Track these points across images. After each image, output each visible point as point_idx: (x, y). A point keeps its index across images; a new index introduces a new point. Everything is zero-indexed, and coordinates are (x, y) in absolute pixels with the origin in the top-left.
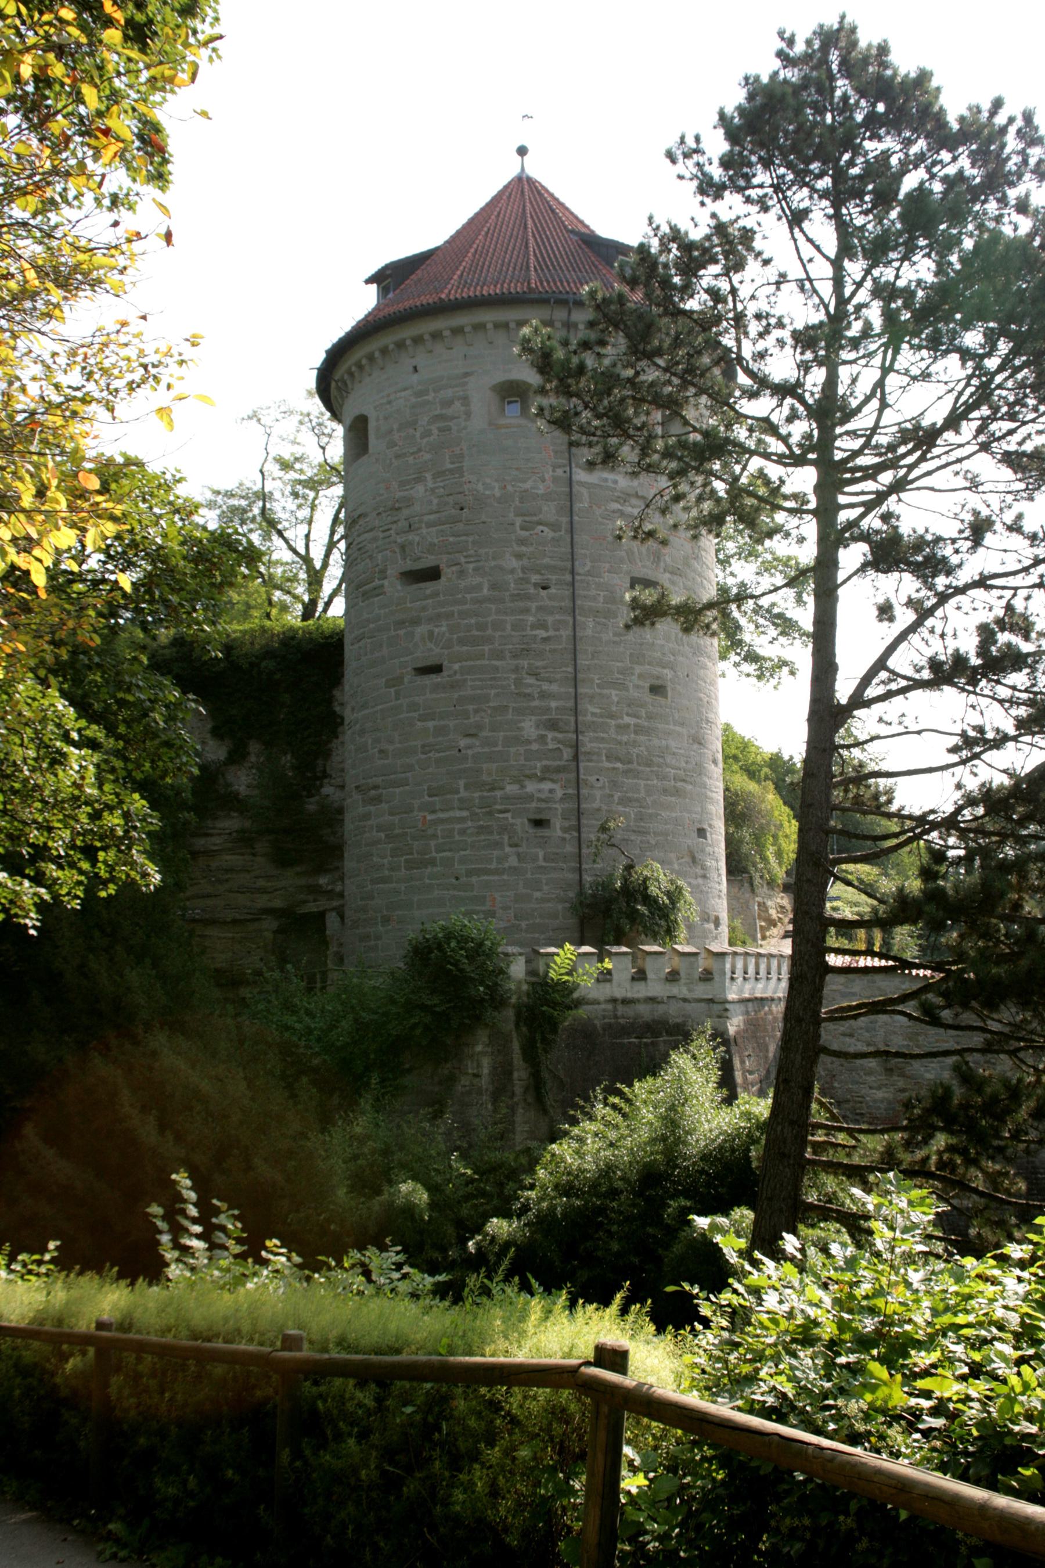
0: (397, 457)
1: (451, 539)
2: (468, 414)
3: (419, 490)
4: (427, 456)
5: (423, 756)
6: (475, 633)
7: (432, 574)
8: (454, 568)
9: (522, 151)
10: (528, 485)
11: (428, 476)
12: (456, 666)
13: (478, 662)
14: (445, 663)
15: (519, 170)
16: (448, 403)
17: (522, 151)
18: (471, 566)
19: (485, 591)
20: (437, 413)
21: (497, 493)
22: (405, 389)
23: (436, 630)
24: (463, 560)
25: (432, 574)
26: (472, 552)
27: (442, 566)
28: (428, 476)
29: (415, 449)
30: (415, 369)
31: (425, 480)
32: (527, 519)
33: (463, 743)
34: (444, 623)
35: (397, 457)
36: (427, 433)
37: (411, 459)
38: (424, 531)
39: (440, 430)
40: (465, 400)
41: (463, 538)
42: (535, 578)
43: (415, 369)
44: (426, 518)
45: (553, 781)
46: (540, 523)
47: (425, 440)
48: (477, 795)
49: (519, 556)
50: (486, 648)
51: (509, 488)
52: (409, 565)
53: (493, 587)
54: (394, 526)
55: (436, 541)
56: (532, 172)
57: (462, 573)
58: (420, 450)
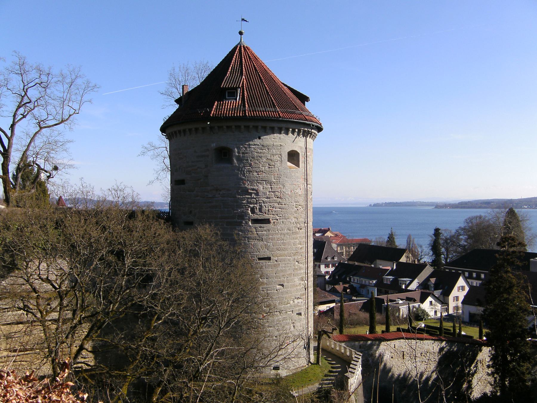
17: (241, 33)
27: (271, 219)
56: (246, 43)
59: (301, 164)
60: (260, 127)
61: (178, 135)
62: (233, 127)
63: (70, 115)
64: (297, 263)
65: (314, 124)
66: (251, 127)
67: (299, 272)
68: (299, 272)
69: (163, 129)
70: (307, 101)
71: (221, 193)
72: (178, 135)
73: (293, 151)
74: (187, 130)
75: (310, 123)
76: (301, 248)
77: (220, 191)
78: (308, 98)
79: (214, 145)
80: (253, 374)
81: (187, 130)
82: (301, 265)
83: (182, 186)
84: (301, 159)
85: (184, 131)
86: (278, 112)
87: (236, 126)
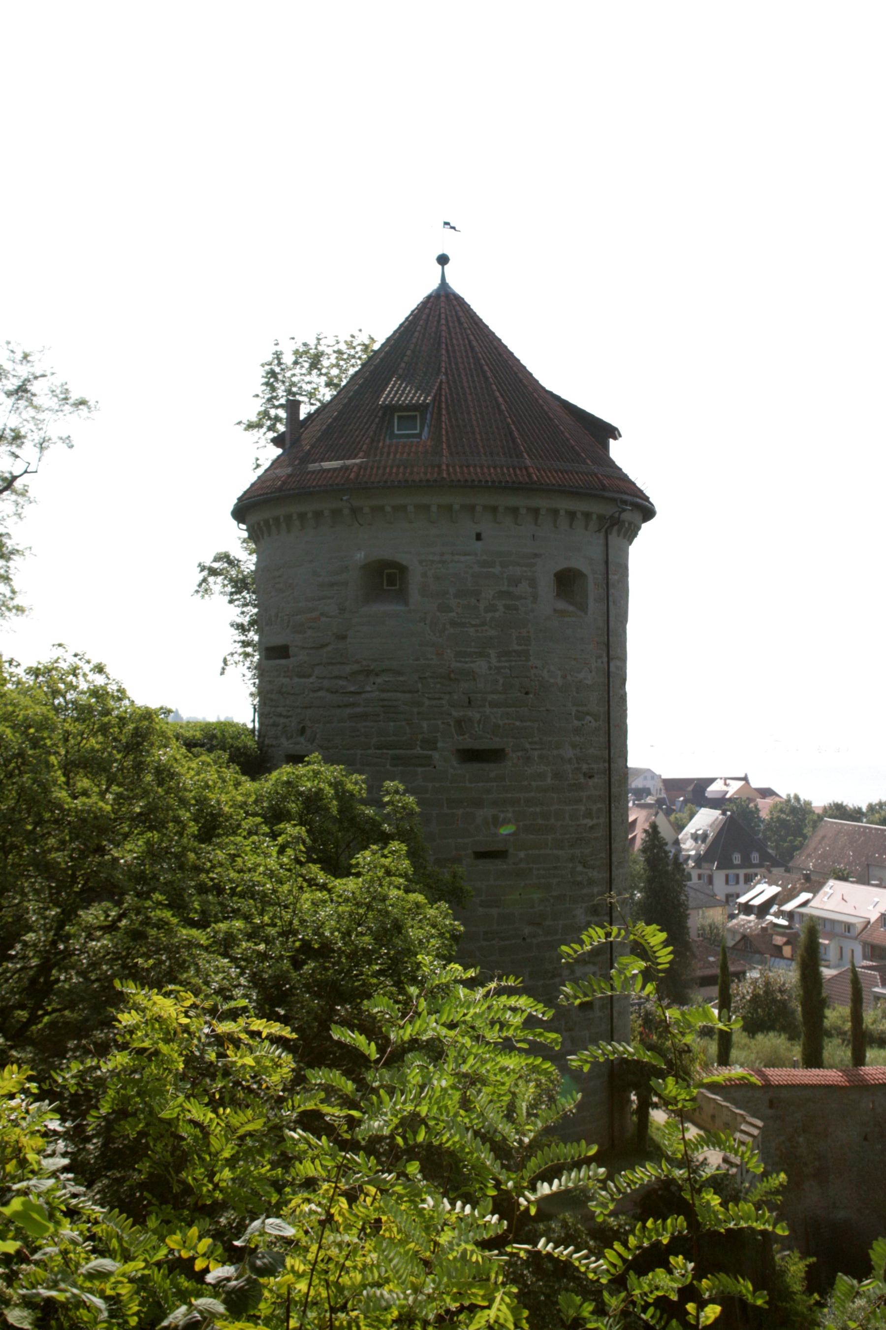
0: (453, 623)
1: (518, 723)
2: (535, 598)
3: (480, 666)
4: (492, 633)
5: (485, 943)
6: (540, 821)
7: (494, 756)
8: (519, 754)
9: (443, 260)
10: (581, 676)
11: (492, 653)
12: (522, 854)
13: (542, 852)
14: (511, 850)
15: (439, 281)
16: (515, 581)
17: (443, 260)
18: (536, 753)
19: (549, 780)
20: (505, 588)
21: (560, 681)
22: (466, 554)
23: (502, 816)
24: (527, 746)
25: (494, 756)
26: (536, 739)
27: (508, 750)
28: (492, 653)
29: (478, 621)
30: (479, 537)
31: (488, 656)
32: (580, 709)
33: (527, 930)
34: (510, 809)
35: (453, 623)
36: (491, 608)
37: (472, 631)
38: (488, 710)
39: (507, 607)
40: (533, 582)
41: (529, 724)
42: (585, 767)
43: (479, 537)
44: (490, 697)
45: (594, 964)
46: (588, 714)
47: (490, 615)
48: (541, 983)
49: (574, 746)
50: (550, 837)
51: (569, 677)
52: (467, 742)
53: (557, 775)
54: (447, 697)
55: (501, 723)
56: (458, 286)
57: (528, 759)
58: (483, 624)
59: (593, 605)
60: (479, 509)
61: (284, 526)
62: (411, 509)
63: (26, 472)
64: (580, 868)
65: (625, 497)
66: (456, 507)
67: (585, 891)
68: (585, 891)
69: (241, 513)
70: (615, 438)
71: (379, 680)
72: (284, 526)
73: (569, 570)
74: (295, 517)
75: (616, 496)
76: (592, 828)
77: (377, 675)
78: (616, 429)
79: (360, 556)
80: (99, 1068)
81: (295, 517)
82: (594, 874)
83: (283, 662)
84: (593, 591)
85: (288, 518)
86: (526, 468)
87: (439, 506)
